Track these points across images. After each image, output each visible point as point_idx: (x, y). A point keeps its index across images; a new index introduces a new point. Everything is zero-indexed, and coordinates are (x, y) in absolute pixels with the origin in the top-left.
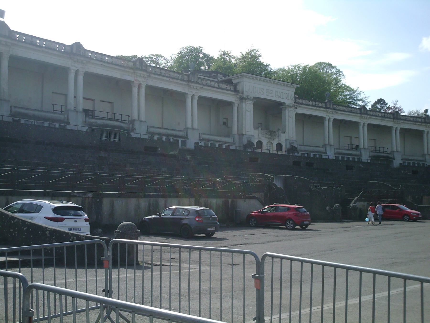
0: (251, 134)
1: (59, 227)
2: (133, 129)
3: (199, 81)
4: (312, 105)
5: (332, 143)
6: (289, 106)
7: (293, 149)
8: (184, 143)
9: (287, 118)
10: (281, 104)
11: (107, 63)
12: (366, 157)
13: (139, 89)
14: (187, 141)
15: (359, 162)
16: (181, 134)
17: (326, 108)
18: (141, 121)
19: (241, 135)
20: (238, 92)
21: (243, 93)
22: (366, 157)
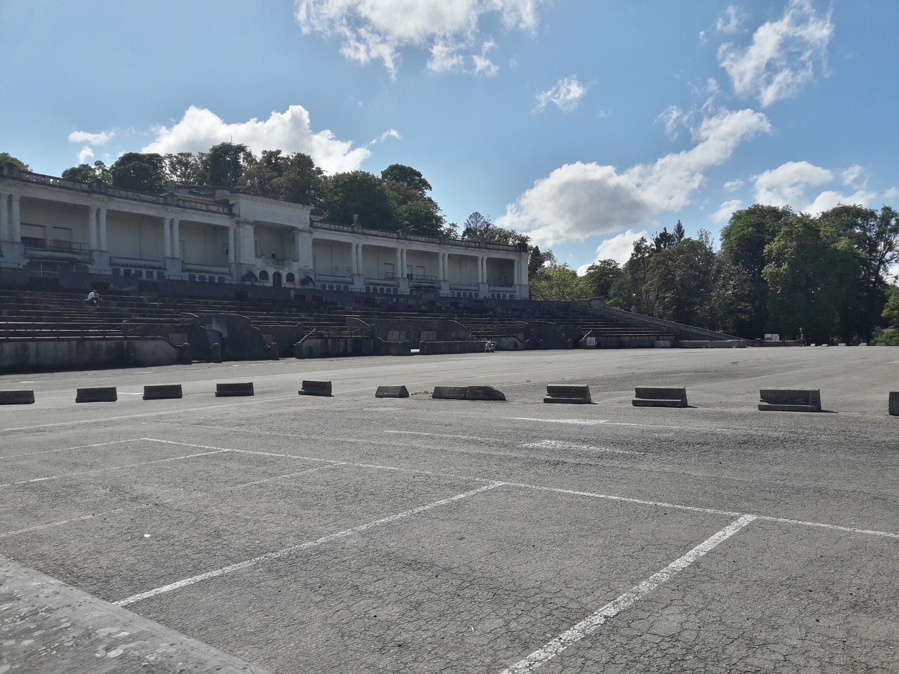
0: (251, 263)
1: (667, 384)
2: (91, 261)
3: (180, 203)
4: (335, 230)
5: (361, 273)
6: (302, 231)
7: (306, 280)
8: (476, 295)
9: (300, 245)
10: (293, 228)
11: (52, 186)
12: (404, 288)
13: (98, 215)
14: (165, 272)
15: (396, 295)
16: (157, 264)
17: (353, 232)
18: (101, 251)
19: (239, 265)
20: (234, 215)
21: (239, 216)
22: (404, 288)
